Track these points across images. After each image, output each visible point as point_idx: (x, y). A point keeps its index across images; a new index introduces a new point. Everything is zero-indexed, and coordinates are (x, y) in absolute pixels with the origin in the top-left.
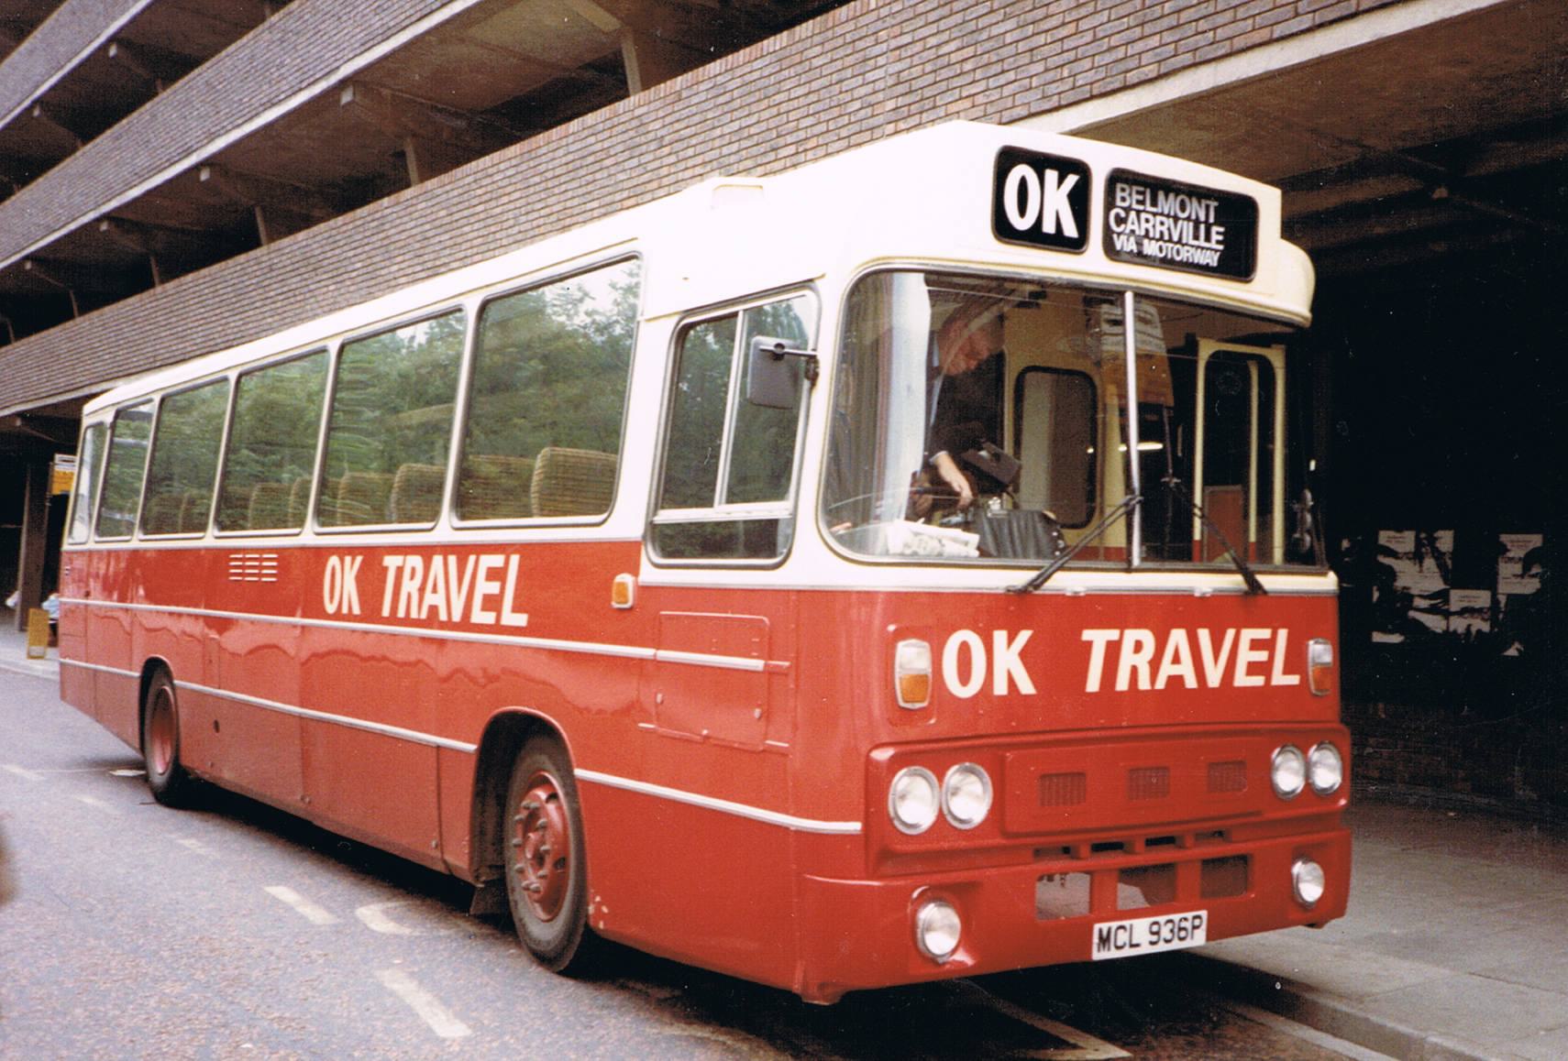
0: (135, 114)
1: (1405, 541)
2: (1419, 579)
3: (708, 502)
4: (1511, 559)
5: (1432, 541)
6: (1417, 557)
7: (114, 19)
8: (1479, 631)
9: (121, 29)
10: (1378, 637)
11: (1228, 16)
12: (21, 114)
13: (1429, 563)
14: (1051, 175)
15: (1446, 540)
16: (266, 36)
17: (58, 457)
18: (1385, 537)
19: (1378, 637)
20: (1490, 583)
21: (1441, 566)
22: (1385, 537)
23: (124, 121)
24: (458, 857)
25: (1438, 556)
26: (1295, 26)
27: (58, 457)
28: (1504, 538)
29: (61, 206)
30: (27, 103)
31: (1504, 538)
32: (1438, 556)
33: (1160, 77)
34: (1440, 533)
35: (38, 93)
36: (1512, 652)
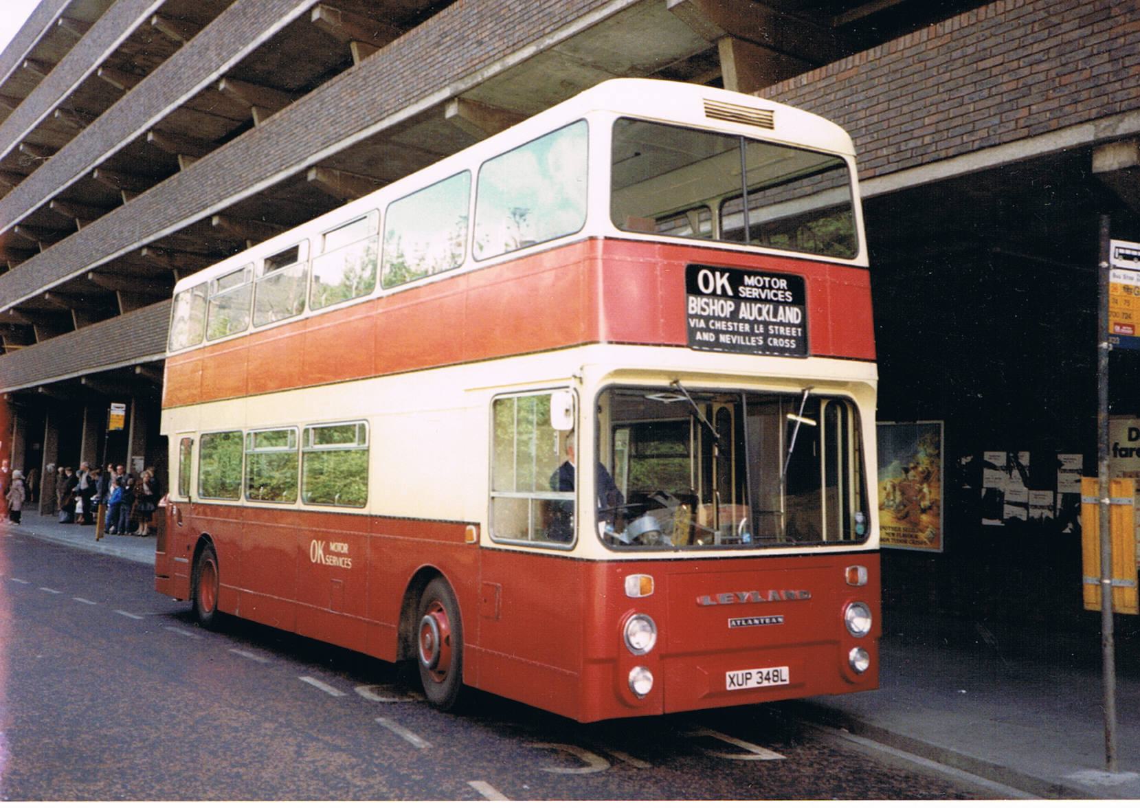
0: (167, 181)
1: (1000, 458)
2: (1012, 487)
3: (802, 424)
4: (1065, 471)
5: (1016, 458)
6: (1008, 469)
7: (151, 116)
8: (1047, 518)
9: (156, 124)
10: (985, 522)
11: (1030, 8)
12: (85, 176)
13: (1016, 473)
14: (718, 274)
15: (1025, 458)
16: (258, 134)
17: (113, 405)
18: (987, 456)
19: (985, 522)
20: (1052, 485)
21: (1023, 474)
22: (987, 456)
23: (159, 185)
24: (390, 654)
25: (1021, 468)
26: (888, 168)
27: (113, 405)
28: (1061, 457)
29: (114, 238)
30: (89, 169)
31: (1061, 457)
32: (1021, 468)
33: (814, 193)
34: (1021, 453)
35: (98, 162)
36: (1067, 531)
